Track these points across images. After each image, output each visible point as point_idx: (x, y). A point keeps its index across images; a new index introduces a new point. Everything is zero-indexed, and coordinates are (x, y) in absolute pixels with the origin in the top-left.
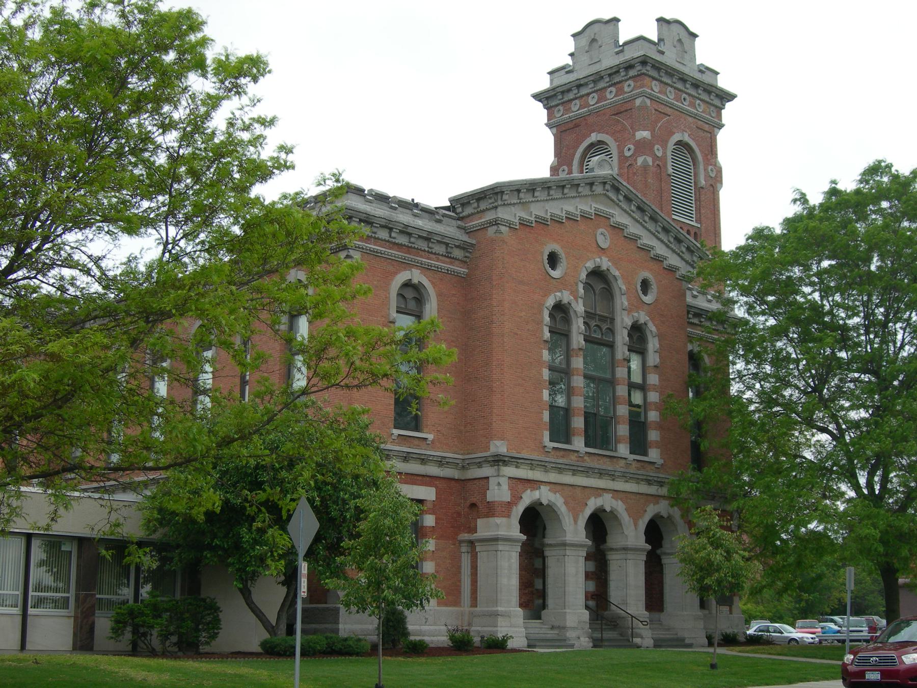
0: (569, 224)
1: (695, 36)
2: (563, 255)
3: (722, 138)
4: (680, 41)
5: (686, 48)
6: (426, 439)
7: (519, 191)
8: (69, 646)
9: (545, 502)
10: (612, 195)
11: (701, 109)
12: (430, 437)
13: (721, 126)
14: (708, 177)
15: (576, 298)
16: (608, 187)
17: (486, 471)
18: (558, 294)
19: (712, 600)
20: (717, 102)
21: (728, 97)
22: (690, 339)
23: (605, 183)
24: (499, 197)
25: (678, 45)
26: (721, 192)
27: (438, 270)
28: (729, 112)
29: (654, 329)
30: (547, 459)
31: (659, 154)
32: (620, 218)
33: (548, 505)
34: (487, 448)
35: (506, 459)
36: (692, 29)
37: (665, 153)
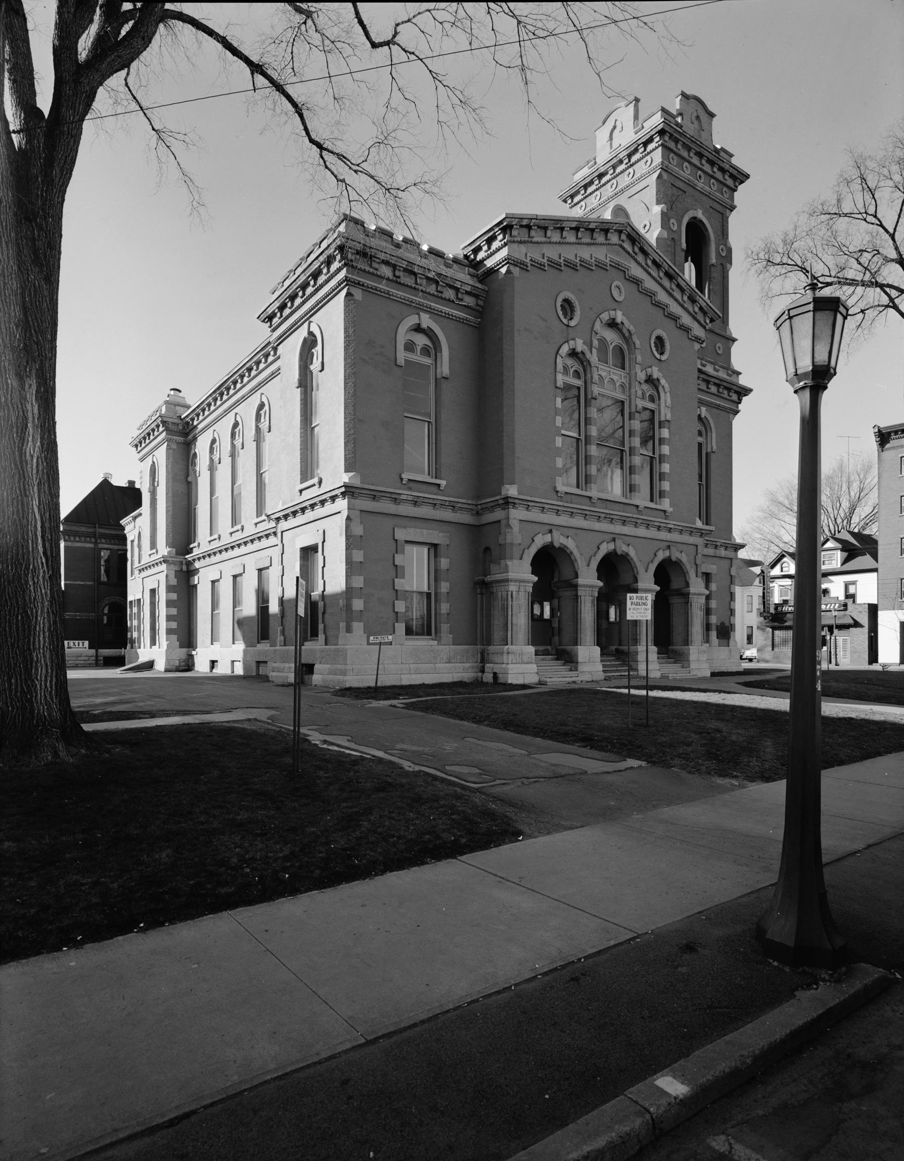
0: (583, 271)
1: (712, 115)
2: (577, 303)
3: (734, 220)
4: (698, 117)
5: (705, 126)
6: (439, 485)
7: (529, 227)
8: (898, 662)
9: (557, 545)
10: (627, 246)
11: (713, 188)
12: (443, 483)
13: (732, 208)
14: (718, 254)
15: (591, 347)
16: (624, 237)
17: (498, 514)
18: (572, 342)
19: (713, 634)
20: (730, 182)
21: (734, 340)
22: (701, 402)
23: (620, 232)
24: (508, 231)
25: (696, 122)
26: (730, 273)
27: (448, 316)
28: (742, 195)
29: (666, 386)
30: (561, 504)
31: (675, 228)
32: (636, 271)
33: (560, 548)
34: (500, 494)
35: (517, 501)
36: (711, 108)
37: (680, 227)
